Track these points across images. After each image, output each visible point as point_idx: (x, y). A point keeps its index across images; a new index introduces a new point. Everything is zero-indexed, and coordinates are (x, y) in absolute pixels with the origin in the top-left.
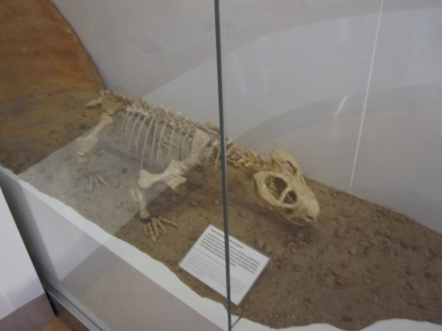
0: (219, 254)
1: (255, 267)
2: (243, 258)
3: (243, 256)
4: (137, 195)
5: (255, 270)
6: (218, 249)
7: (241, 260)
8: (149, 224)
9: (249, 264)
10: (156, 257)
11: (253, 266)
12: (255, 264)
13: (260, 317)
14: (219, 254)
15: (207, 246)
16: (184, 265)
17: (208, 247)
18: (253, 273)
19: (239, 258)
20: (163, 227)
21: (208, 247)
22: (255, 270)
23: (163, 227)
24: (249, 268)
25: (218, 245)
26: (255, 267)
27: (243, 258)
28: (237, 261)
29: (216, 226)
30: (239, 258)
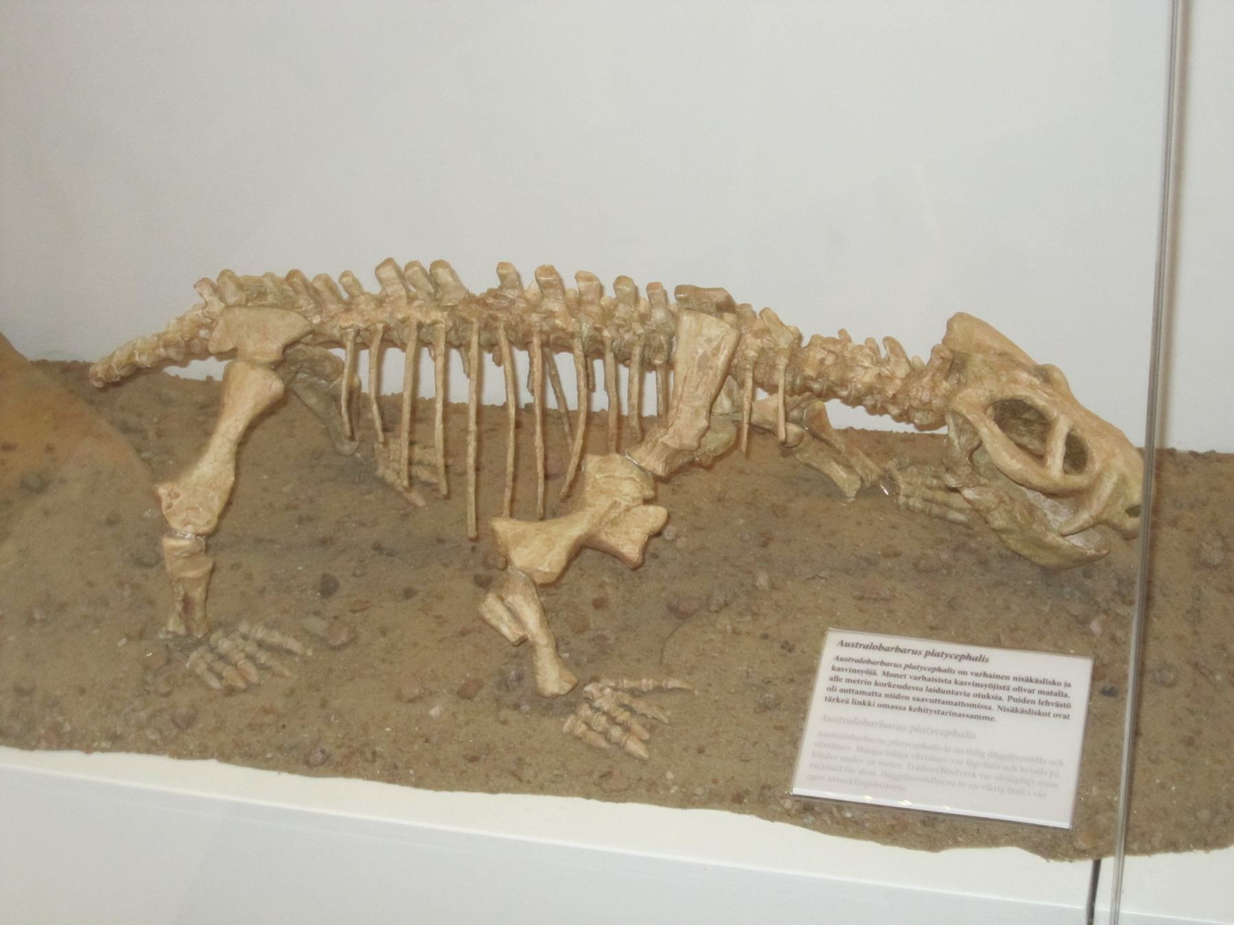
0: (915, 705)
1: (1062, 700)
2: (1007, 688)
3: (1001, 682)
4: (516, 617)
5: (1068, 706)
6: (903, 692)
7: (1003, 694)
8: (585, 711)
9: (1035, 697)
10: (686, 800)
11: (1051, 699)
12: (1055, 694)
13: (1225, 655)
14: (915, 705)
15: (860, 698)
16: (802, 787)
17: (867, 698)
18: (1066, 717)
19: (992, 692)
20: (640, 706)
21: (867, 698)
22: (1068, 706)
23: (640, 706)
24: (1044, 709)
25: (894, 681)
26: (1062, 700)
27: (1007, 688)
28: (994, 703)
29: (841, 625)
30: (992, 692)
